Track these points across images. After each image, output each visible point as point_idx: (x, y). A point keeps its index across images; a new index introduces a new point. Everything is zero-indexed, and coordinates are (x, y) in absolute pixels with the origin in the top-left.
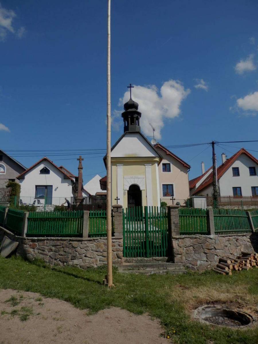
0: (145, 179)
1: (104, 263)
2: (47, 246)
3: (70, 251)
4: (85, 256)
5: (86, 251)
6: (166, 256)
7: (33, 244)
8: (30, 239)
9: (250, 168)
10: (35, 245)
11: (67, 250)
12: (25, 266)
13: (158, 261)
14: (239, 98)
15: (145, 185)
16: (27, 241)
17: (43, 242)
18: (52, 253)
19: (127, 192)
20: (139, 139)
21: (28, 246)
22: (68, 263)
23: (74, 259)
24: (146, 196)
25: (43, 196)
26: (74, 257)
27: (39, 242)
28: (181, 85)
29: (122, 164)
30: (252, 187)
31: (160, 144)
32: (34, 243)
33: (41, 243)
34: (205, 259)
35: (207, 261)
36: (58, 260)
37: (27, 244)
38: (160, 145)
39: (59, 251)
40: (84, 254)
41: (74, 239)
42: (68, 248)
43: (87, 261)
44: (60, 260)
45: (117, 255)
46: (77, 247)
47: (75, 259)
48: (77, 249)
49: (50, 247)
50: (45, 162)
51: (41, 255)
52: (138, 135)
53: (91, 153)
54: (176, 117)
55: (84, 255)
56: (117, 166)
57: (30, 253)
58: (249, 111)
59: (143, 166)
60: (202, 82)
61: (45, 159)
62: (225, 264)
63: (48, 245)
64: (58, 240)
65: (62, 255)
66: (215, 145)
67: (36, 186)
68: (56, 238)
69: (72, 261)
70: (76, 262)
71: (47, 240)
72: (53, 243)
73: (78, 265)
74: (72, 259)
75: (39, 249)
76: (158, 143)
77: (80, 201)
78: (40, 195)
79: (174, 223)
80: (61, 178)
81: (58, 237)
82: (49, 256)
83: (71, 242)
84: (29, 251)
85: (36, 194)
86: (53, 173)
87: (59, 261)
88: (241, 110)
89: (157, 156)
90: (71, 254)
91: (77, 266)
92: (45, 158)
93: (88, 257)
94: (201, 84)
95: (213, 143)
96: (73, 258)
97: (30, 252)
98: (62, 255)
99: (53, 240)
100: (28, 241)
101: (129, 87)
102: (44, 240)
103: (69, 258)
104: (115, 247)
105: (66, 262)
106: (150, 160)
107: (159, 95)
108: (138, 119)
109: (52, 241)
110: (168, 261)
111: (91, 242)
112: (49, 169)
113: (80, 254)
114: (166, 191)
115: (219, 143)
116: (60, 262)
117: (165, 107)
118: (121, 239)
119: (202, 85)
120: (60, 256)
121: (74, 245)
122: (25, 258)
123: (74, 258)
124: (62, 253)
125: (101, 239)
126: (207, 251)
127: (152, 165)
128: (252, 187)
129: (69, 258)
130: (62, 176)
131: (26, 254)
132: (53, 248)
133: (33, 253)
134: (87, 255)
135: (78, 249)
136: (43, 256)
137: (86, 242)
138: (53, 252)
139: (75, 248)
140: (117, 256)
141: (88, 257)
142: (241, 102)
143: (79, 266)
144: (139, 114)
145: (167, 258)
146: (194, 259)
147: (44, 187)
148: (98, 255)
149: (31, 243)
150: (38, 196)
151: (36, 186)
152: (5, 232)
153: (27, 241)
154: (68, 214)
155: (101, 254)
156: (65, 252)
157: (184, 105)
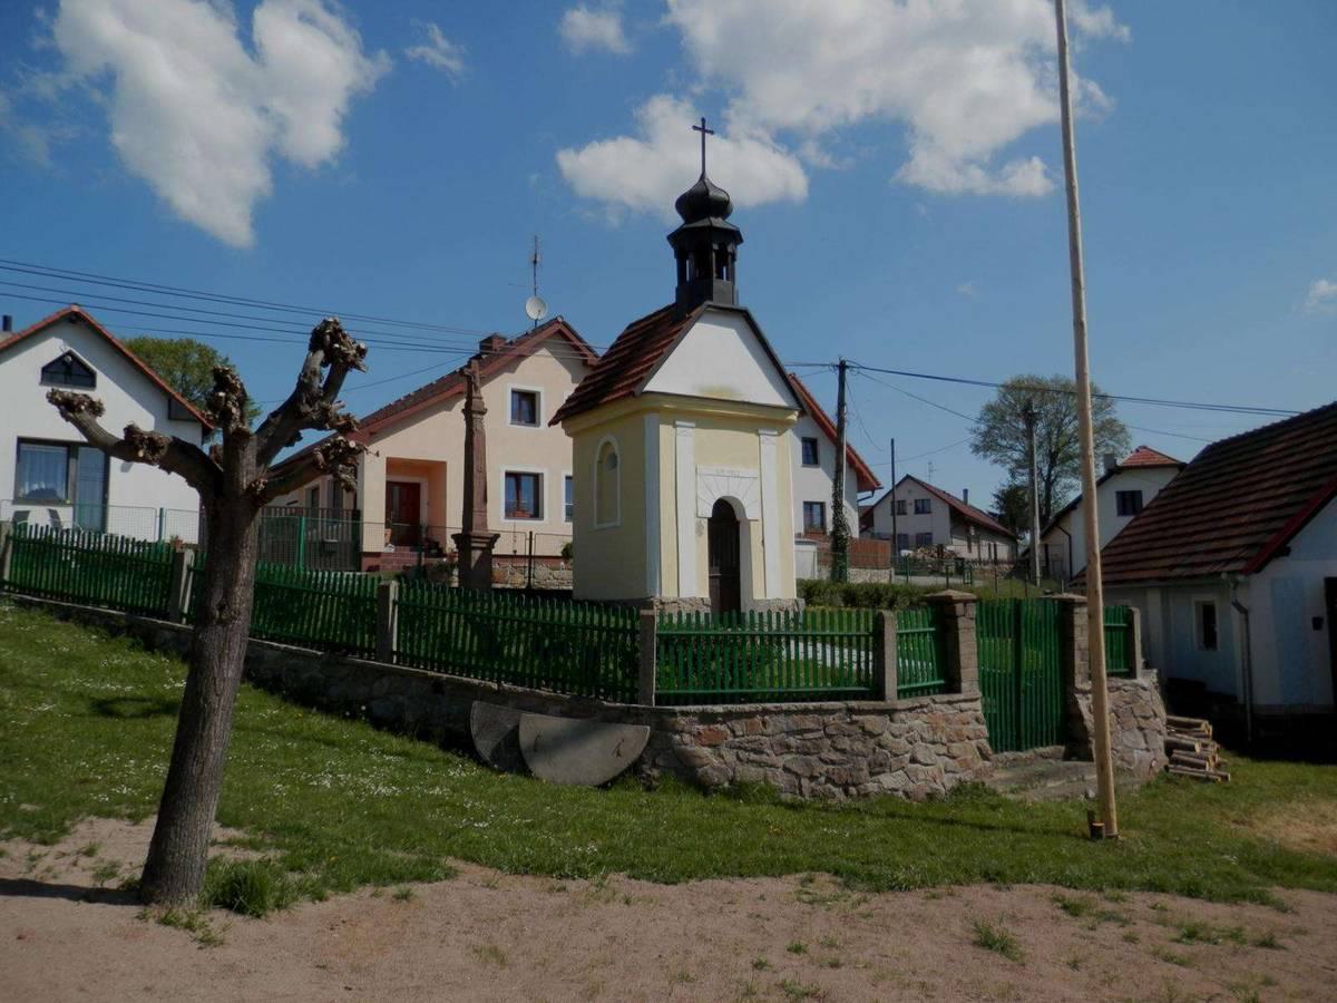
0: (758, 482)
1: (958, 776)
2: (768, 736)
3: (858, 746)
4: (913, 760)
5: (911, 743)
6: (1058, 744)
7: (710, 730)
8: (694, 714)
9: (805, 440)
10: (718, 732)
11: (845, 743)
12: (689, 804)
13: (1047, 758)
14: (565, 146)
15: (759, 504)
16: (683, 722)
17: (749, 721)
18: (789, 757)
19: (705, 523)
20: (741, 334)
21: (687, 738)
22: (862, 787)
23: (879, 773)
24: (763, 541)
25: (52, 492)
26: (881, 765)
27: (733, 722)
28: (350, 23)
29: (690, 421)
30: (806, 503)
31: (566, 320)
32: (712, 727)
33: (739, 727)
34: (1144, 745)
35: (1148, 750)
36: (823, 779)
37: (682, 732)
38: (565, 324)
39: (819, 749)
40: (907, 752)
41: (866, 708)
42: (849, 736)
43: (922, 776)
44: (829, 780)
45: (979, 749)
46: (880, 731)
47: (884, 772)
48: (881, 738)
49: (778, 737)
50: (69, 330)
51: (753, 769)
52: (741, 323)
53: (135, 286)
54: (324, 165)
55: (908, 756)
56: (675, 426)
57: (707, 765)
58: (596, 204)
59: (753, 435)
60: (436, 32)
61: (76, 314)
62: (1192, 754)
63: (769, 730)
64: (806, 712)
65: (833, 762)
66: (847, 371)
67: (21, 440)
68: (797, 704)
69: (875, 778)
70: (888, 780)
71: (765, 712)
72: (787, 724)
73: (896, 790)
74: (872, 774)
75: (740, 748)
76: (560, 320)
77: (484, 545)
78: (36, 487)
79: (1080, 649)
80: (153, 414)
81: (777, 701)
82: (780, 770)
83: (855, 717)
84: (701, 758)
85: (19, 482)
86: (107, 379)
87: (826, 782)
88: (564, 190)
89: (792, 403)
90: (864, 756)
91: (895, 793)
92: (76, 309)
93: (920, 763)
94: (433, 44)
95: (842, 367)
96: (877, 769)
97: (705, 761)
98: (833, 762)
99: (788, 713)
100: (687, 719)
101: (704, 126)
102: (750, 715)
103: (862, 770)
104: (971, 726)
105: (854, 785)
106: (778, 416)
107: (246, 37)
108: (726, 259)
109: (781, 718)
110: (1067, 757)
111: (913, 714)
112: (94, 368)
113: (896, 755)
114: (513, 500)
115: (862, 371)
116: (829, 785)
117: (277, 104)
118: (976, 700)
119: (439, 52)
120: (825, 767)
121: (868, 727)
122: (690, 777)
123: (877, 768)
124: (835, 756)
125: (934, 702)
126: (1143, 723)
127: (780, 434)
128: (806, 503)
129: (862, 770)
130: (162, 407)
131: (693, 768)
132: (792, 741)
133: (716, 762)
134: (920, 757)
135: (887, 738)
136: (761, 770)
137: (902, 715)
138: (794, 756)
139: (872, 735)
140: (981, 753)
141: (920, 763)
142: (568, 161)
143: (901, 793)
144: (735, 236)
145: (1063, 748)
146: (1126, 746)
147: (63, 450)
148: (939, 755)
149: (701, 727)
150: (27, 491)
151: (21, 440)
152: (469, 687)
153: (682, 721)
154: (823, 622)
155: (943, 750)
156: (843, 751)
157: (360, 116)
